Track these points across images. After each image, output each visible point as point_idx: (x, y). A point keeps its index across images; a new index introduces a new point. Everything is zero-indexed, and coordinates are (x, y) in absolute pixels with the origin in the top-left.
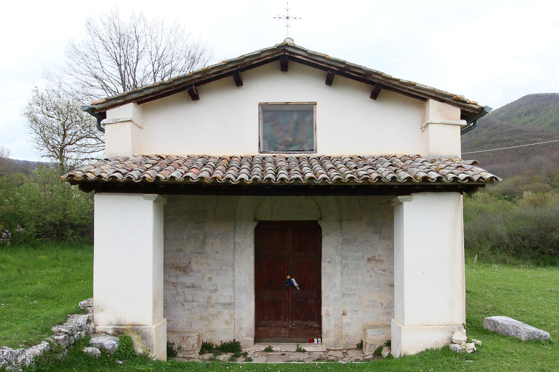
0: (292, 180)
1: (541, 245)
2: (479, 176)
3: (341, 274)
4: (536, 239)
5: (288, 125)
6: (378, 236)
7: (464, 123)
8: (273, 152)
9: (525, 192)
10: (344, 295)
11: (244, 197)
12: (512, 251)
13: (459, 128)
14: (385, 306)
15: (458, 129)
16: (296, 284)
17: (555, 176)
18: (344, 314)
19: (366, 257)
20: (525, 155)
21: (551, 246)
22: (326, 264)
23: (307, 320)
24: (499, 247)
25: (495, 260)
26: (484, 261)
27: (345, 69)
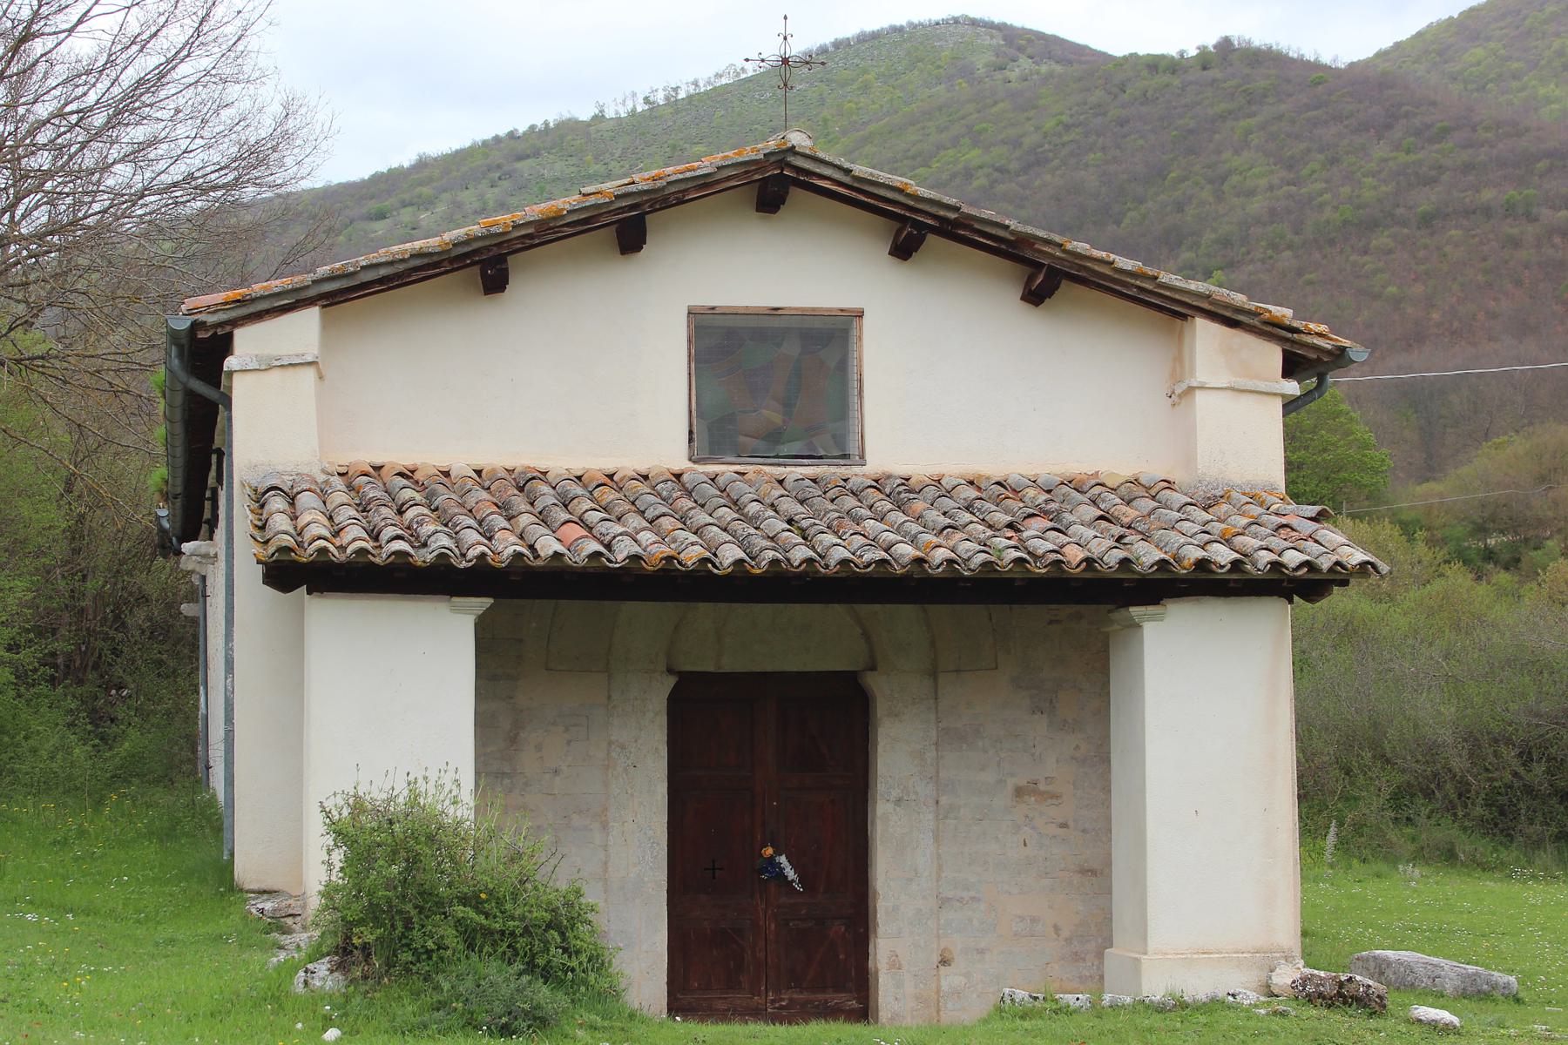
0: (869, 565)
2: (1334, 558)
5: (776, 383)
7: (1292, 388)
8: (733, 459)
10: (943, 902)
12: (1479, 811)
14: (1065, 933)
15: (1277, 406)
16: (790, 873)
18: (944, 962)
19: (1011, 783)
22: (890, 807)
24: (1429, 795)
25: (1411, 847)
27: (956, 224)
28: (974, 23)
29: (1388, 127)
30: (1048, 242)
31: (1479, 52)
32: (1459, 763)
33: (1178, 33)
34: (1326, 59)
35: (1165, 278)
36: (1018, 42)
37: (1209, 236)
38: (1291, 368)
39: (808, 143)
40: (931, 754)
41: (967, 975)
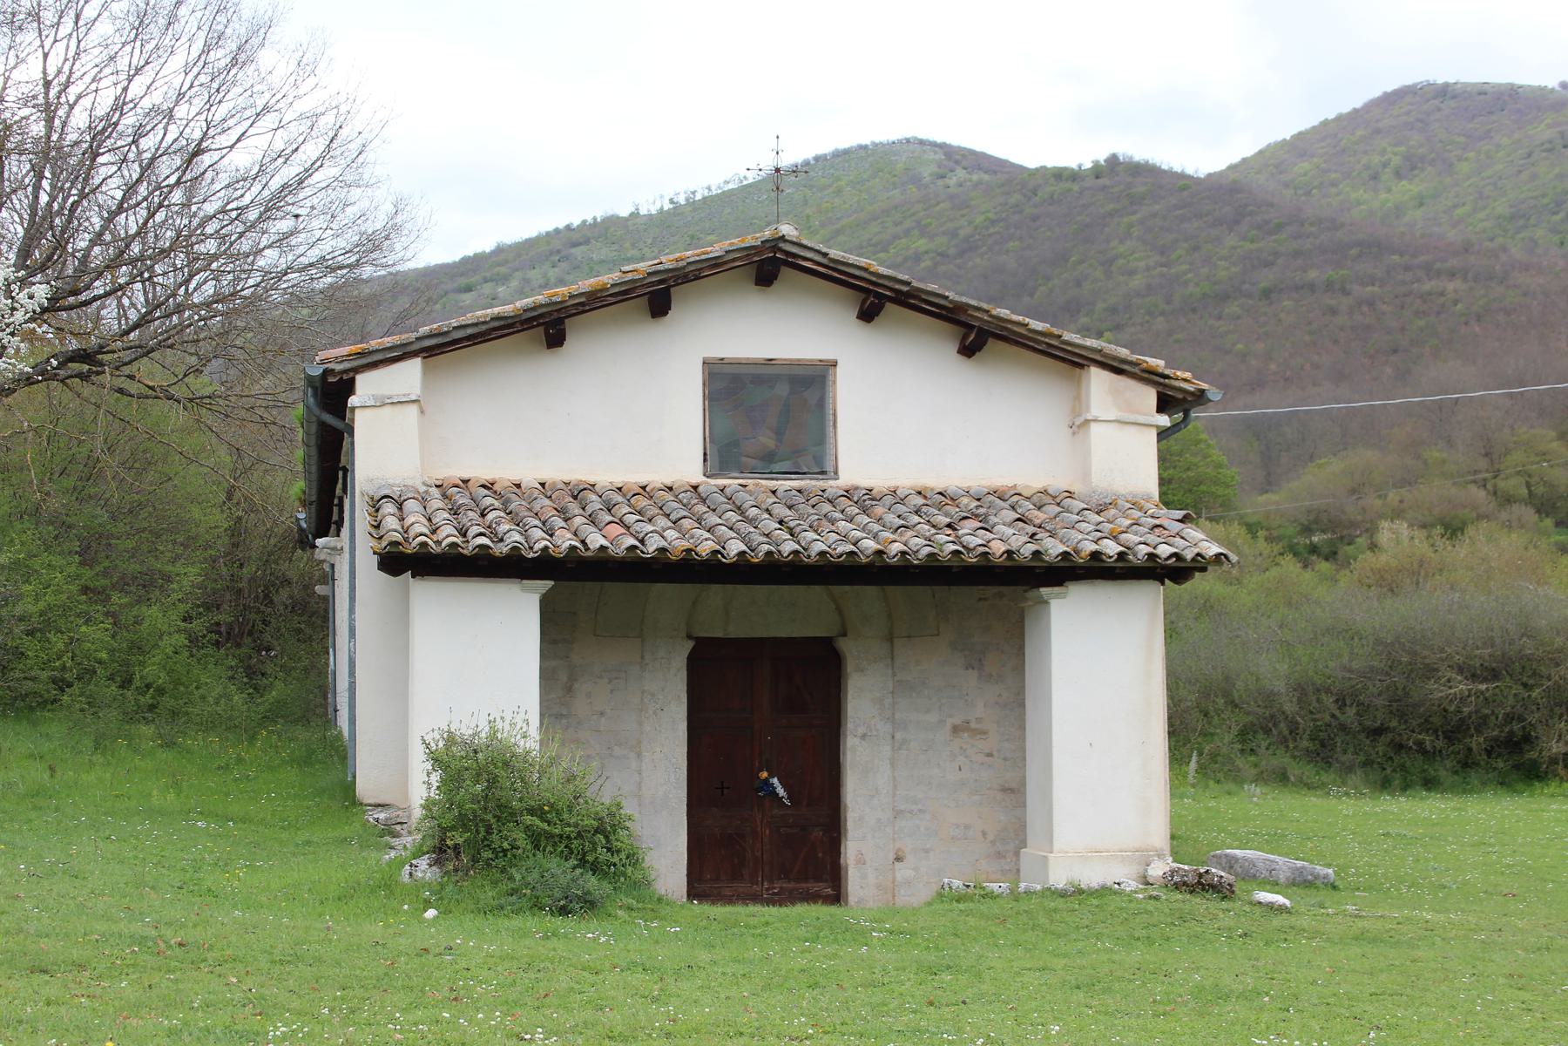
1: (1394, 724)
2: (1196, 551)
3: (892, 764)
4: (1380, 702)
5: (769, 416)
6: (975, 673)
7: (1164, 420)
9: (1385, 524)
10: (898, 814)
11: (659, 586)
12: (1305, 744)
13: (1154, 433)
14: (991, 837)
16: (781, 791)
17: (1508, 452)
18: (898, 859)
19: (950, 722)
20: (1395, 351)
21: (1426, 726)
22: (857, 741)
23: (806, 880)
24: (1268, 732)
25: (1254, 771)
26: (1220, 775)
27: (908, 295)
28: (922, 142)
29: (1237, 222)
30: (978, 309)
31: (1305, 165)
32: (1290, 708)
33: (1081, 153)
34: (1190, 171)
35: (1067, 336)
36: (954, 157)
37: (1100, 306)
38: (1164, 405)
39: (795, 233)
40: (888, 701)
41: (916, 869)
